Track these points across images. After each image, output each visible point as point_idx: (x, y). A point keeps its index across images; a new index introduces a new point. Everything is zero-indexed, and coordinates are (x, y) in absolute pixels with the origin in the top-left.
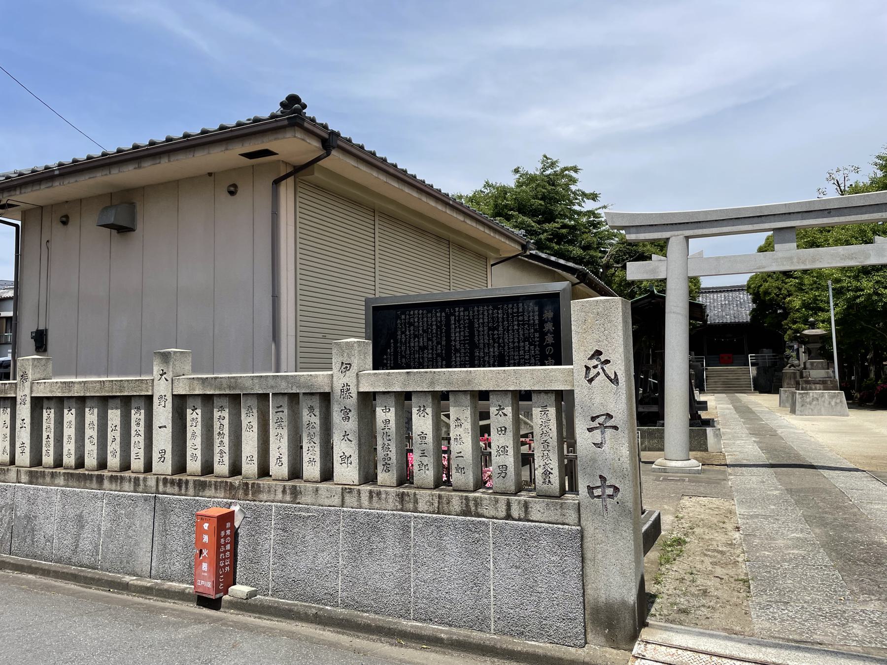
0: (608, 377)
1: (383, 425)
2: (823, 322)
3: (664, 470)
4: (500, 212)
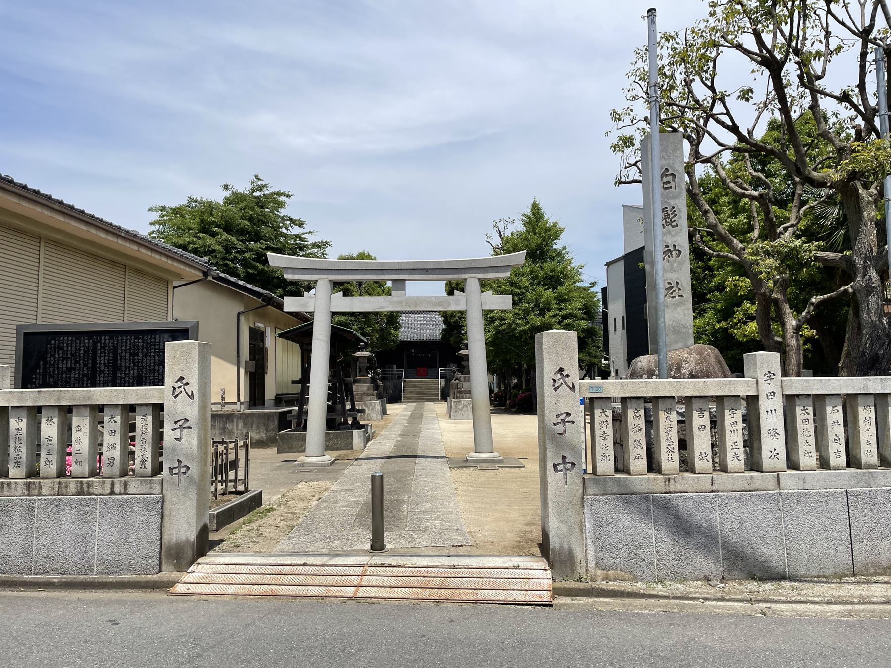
0: (568, 387)
1: (16, 432)
3: (303, 465)
4: (206, 228)
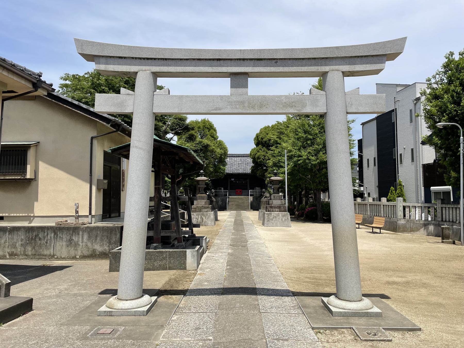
2: (282, 173)
